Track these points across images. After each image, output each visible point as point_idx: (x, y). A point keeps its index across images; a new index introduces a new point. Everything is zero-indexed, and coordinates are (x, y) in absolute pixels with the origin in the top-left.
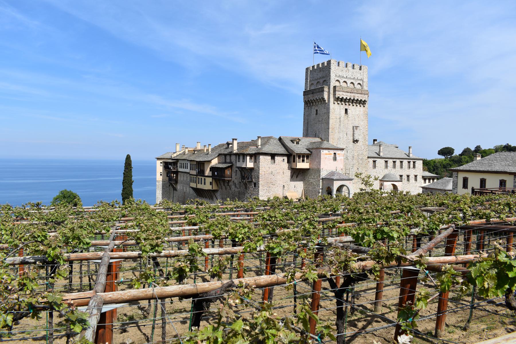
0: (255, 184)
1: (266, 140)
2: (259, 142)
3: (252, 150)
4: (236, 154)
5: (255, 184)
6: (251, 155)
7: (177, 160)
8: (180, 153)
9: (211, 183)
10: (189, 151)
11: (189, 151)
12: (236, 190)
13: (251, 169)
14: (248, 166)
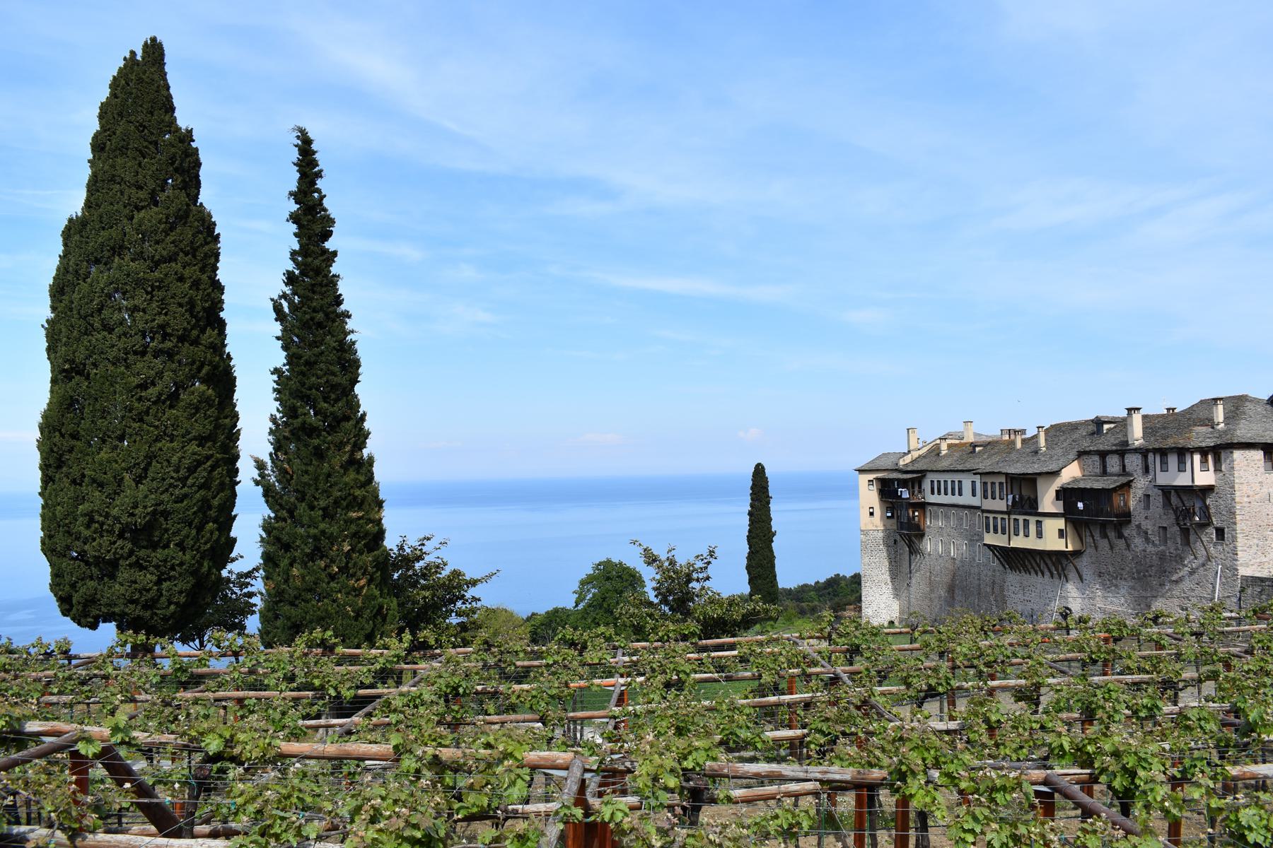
0: (1220, 533)
1: (1237, 405)
2: (1219, 413)
3: (1200, 436)
4: (1144, 452)
5: (1220, 533)
6: (1204, 452)
7: (923, 473)
8: (921, 452)
9: (1061, 534)
10: (950, 446)
11: (950, 446)
12: (1150, 548)
13: (1209, 489)
14: (1197, 483)
